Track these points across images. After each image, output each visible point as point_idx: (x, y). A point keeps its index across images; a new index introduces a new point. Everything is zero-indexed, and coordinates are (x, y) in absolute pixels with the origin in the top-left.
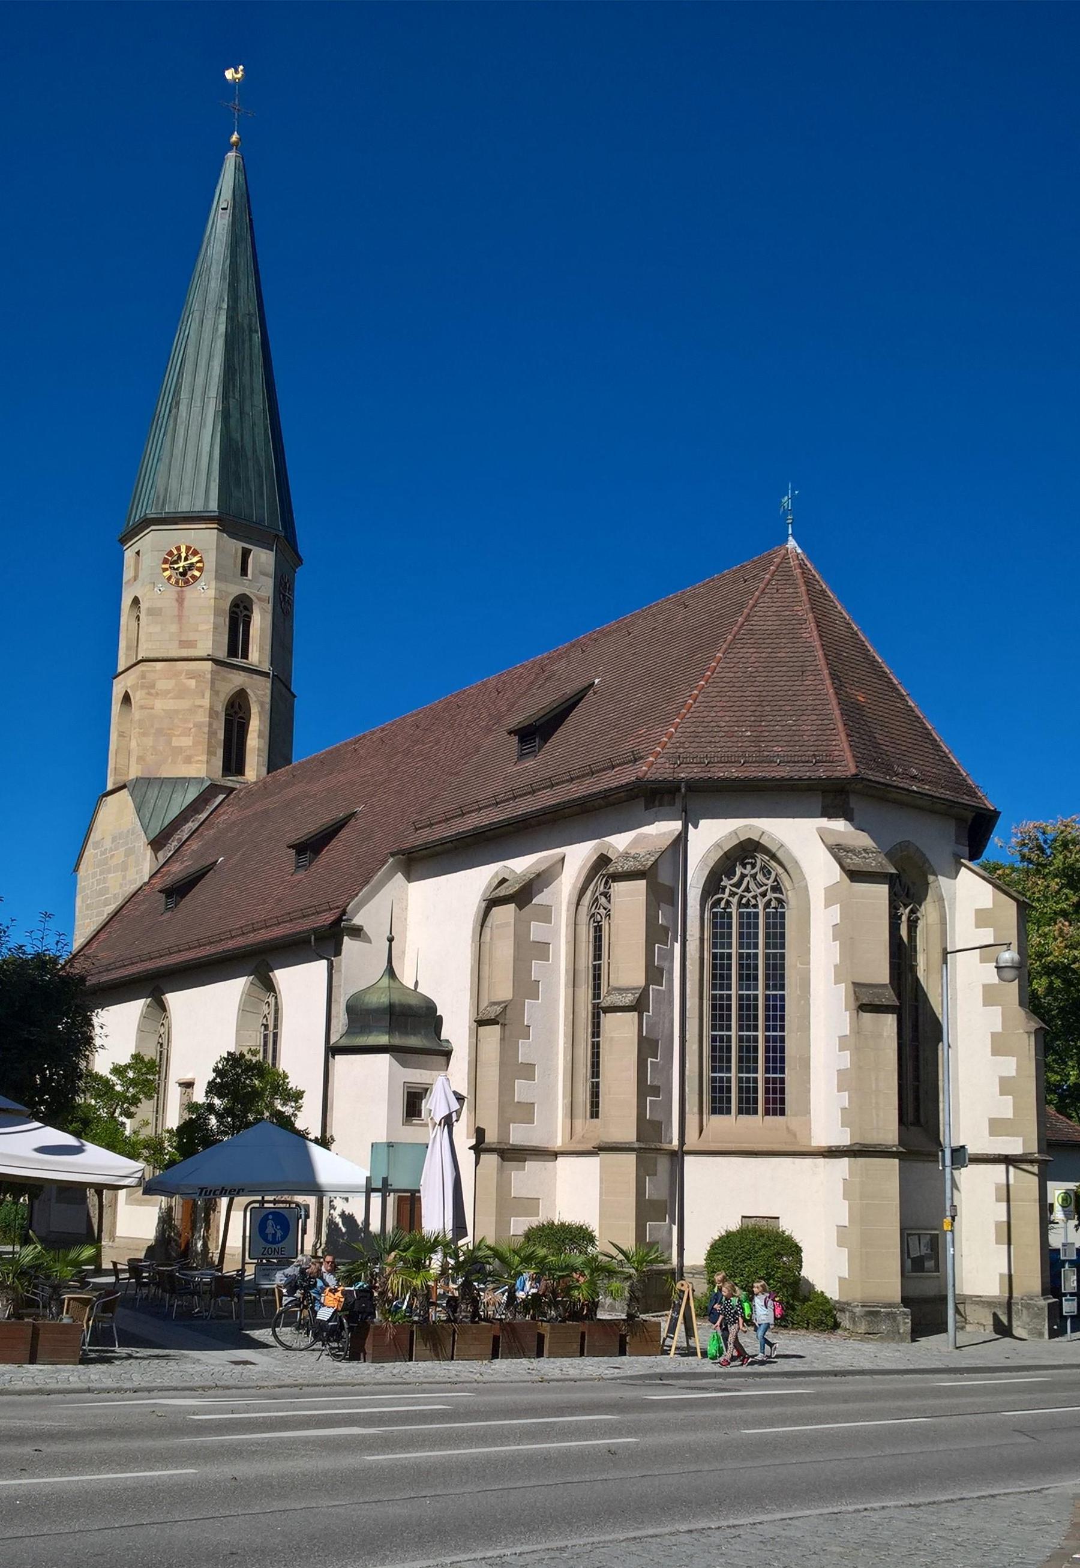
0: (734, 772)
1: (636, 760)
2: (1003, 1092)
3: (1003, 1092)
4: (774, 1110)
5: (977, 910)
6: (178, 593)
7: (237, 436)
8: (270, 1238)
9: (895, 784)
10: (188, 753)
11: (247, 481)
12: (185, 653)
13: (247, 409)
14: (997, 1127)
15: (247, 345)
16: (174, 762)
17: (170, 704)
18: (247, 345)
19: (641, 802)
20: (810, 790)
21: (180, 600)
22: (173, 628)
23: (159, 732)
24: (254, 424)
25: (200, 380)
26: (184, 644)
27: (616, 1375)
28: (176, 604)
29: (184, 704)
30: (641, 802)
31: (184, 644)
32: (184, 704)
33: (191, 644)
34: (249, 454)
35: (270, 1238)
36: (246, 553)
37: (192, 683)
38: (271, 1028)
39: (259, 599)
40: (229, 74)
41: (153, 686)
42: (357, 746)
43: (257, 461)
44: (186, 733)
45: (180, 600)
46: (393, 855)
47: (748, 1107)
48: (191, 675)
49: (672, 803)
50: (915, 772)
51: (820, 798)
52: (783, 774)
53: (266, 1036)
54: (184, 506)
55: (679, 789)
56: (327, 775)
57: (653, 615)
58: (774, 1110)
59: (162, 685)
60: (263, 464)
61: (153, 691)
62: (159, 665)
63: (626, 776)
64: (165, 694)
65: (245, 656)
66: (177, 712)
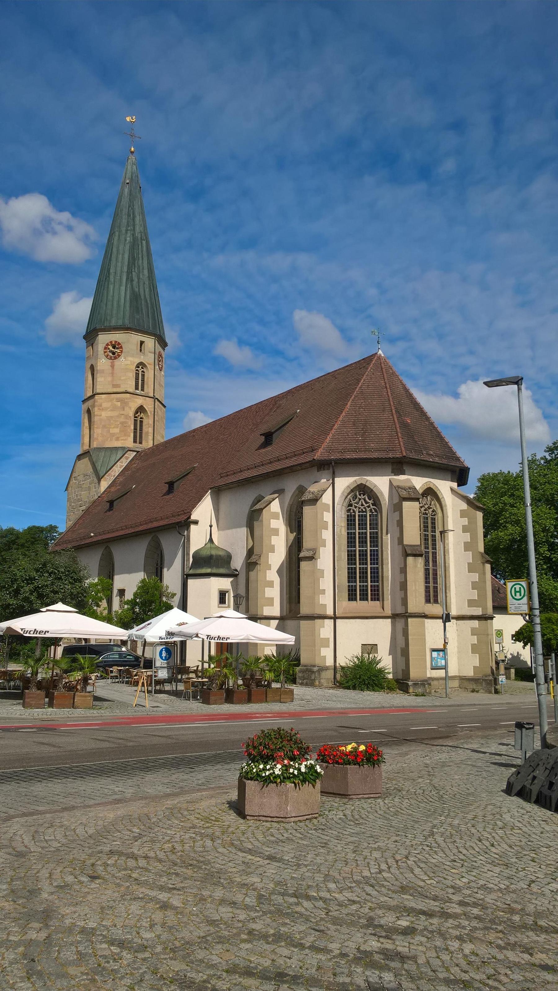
0: (355, 456)
1: (313, 450)
2: (473, 588)
3: (473, 588)
4: (375, 598)
5: (461, 510)
6: (111, 362)
7: (137, 290)
8: (164, 658)
9: (422, 459)
10: (118, 436)
11: (142, 310)
12: (115, 390)
13: (141, 276)
14: (471, 603)
15: (140, 247)
16: (111, 440)
17: (109, 414)
18: (140, 247)
19: (316, 468)
20: (386, 462)
21: (113, 366)
22: (109, 379)
23: (104, 427)
24: (144, 283)
25: (119, 264)
26: (114, 386)
27: (441, 740)
28: (111, 368)
29: (115, 413)
30: (316, 468)
31: (114, 386)
32: (115, 413)
33: (118, 386)
34: (143, 297)
35: (164, 658)
36: (142, 343)
37: (119, 404)
38: (159, 564)
39: (149, 364)
40: (128, 119)
41: (101, 406)
42: (195, 434)
43: (146, 301)
44: (116, 427)
45: (113, 366)
46: (211, 489)
47: (364, 598)
48: (118, 400)
49: (328, 469)
50: (432, 453)
51: (391, 466)
52: (375, 456)
53: (157, 568)
54: (113, 323)
55: (331, 463)
56: (181, 447)
57: (323, 381)
58: (375, 598)
59: (105, 405)
60: (149, 302)
61: (101, 408)
62: (103, 396)
63: (308, 458)
64: (105, 409)
65: (143, 390)
66: (112, 417)
